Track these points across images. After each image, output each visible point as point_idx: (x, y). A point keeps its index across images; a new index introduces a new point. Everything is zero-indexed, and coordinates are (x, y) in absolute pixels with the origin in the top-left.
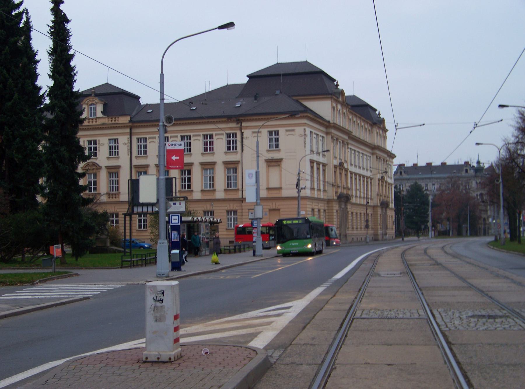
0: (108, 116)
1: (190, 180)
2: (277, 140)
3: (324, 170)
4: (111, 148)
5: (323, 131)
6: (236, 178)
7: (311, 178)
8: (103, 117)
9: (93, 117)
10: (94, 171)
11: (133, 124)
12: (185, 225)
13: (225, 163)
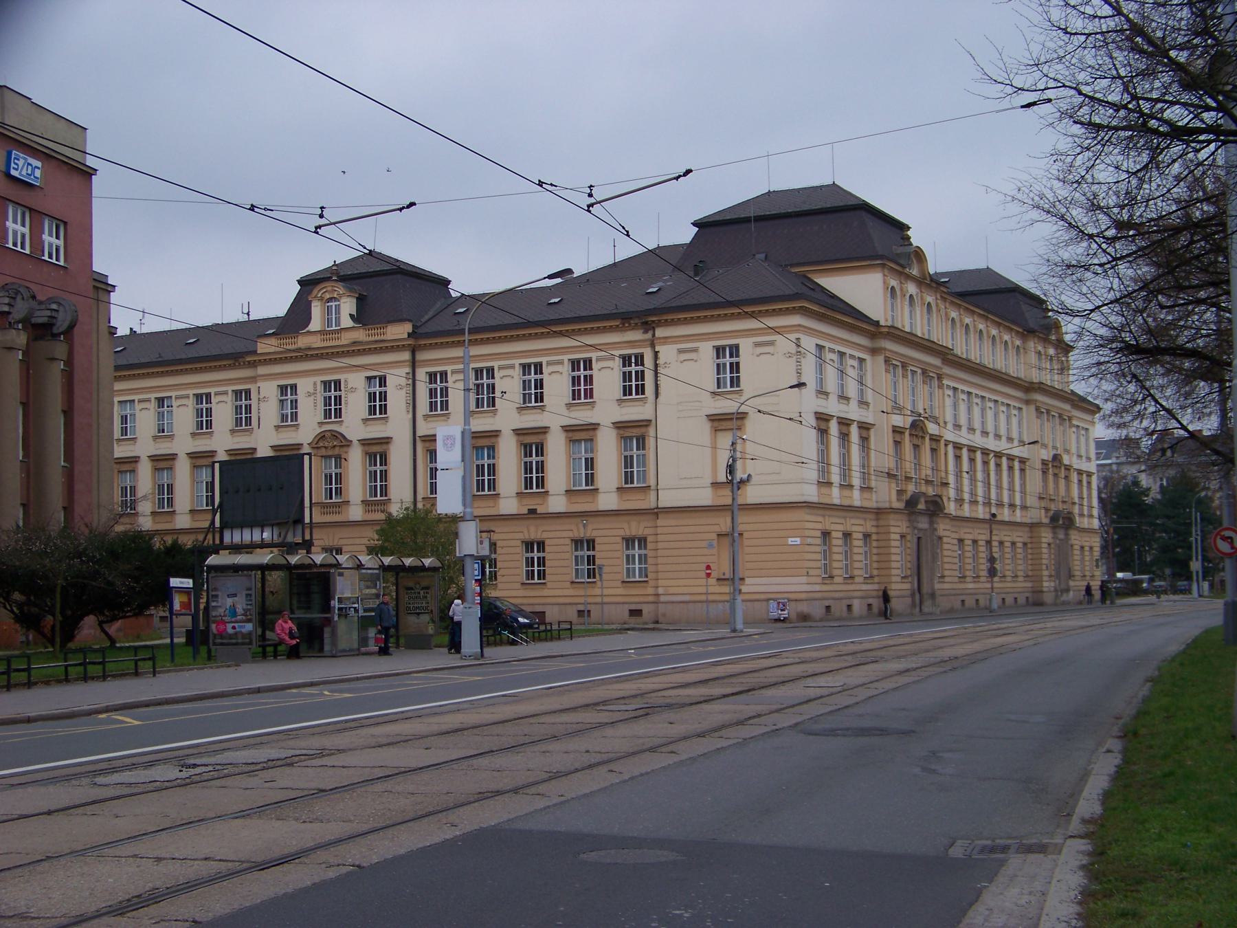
0: (364, 325)
1: (541, 467)
2: (735, 367)
3: (1022, 470)
4: (372, 397)
5: (1018, 398)
6: (643, 461)
7: (957, 479)
8: (353, 327)
9: (334, 328)
10: (337, 451)
11: (419, 341)
12: (250, 576)
13: (619, 426)
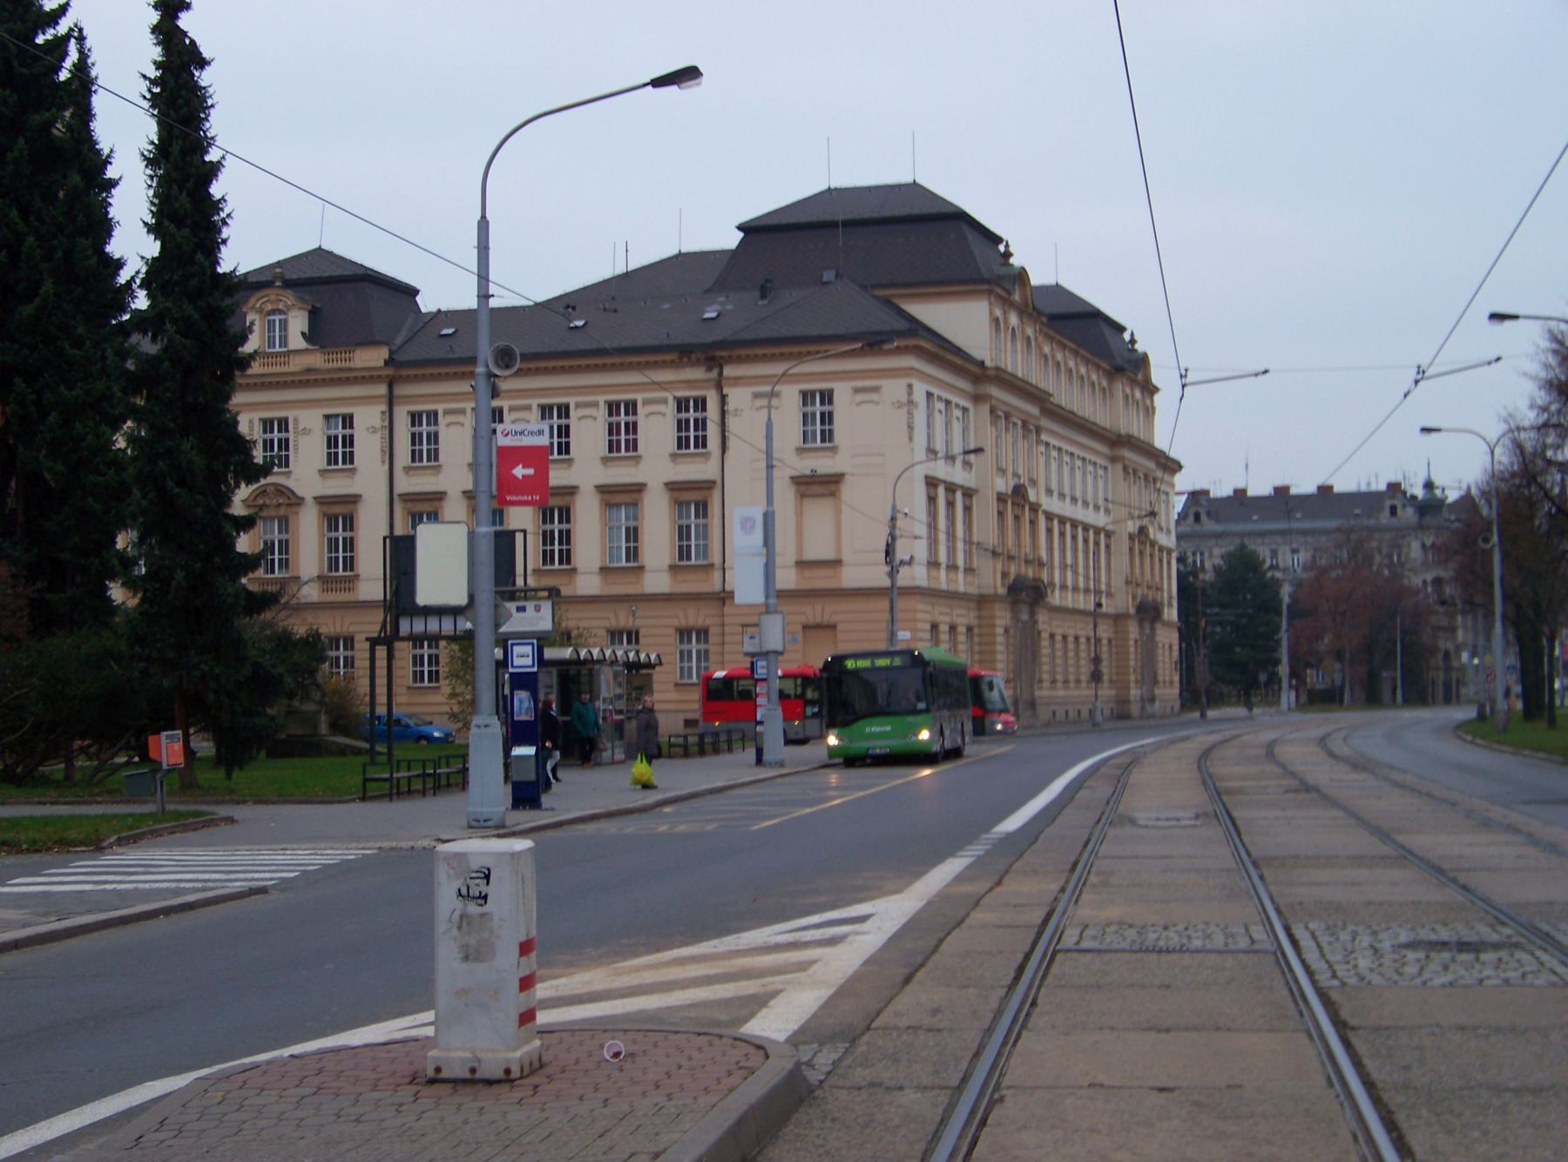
0: (322, 347)
1: (566, 537)
2: (827, 418)
3: (968, 509)
4: (332, 442)
5: (965, 392)
6: (704, 532)
7: (930, 532)
8: (307, 350)
9: (277, 349)
10: (282, 511)
11: (398, 372)
12: (551, 673)
13: (672, 487)
